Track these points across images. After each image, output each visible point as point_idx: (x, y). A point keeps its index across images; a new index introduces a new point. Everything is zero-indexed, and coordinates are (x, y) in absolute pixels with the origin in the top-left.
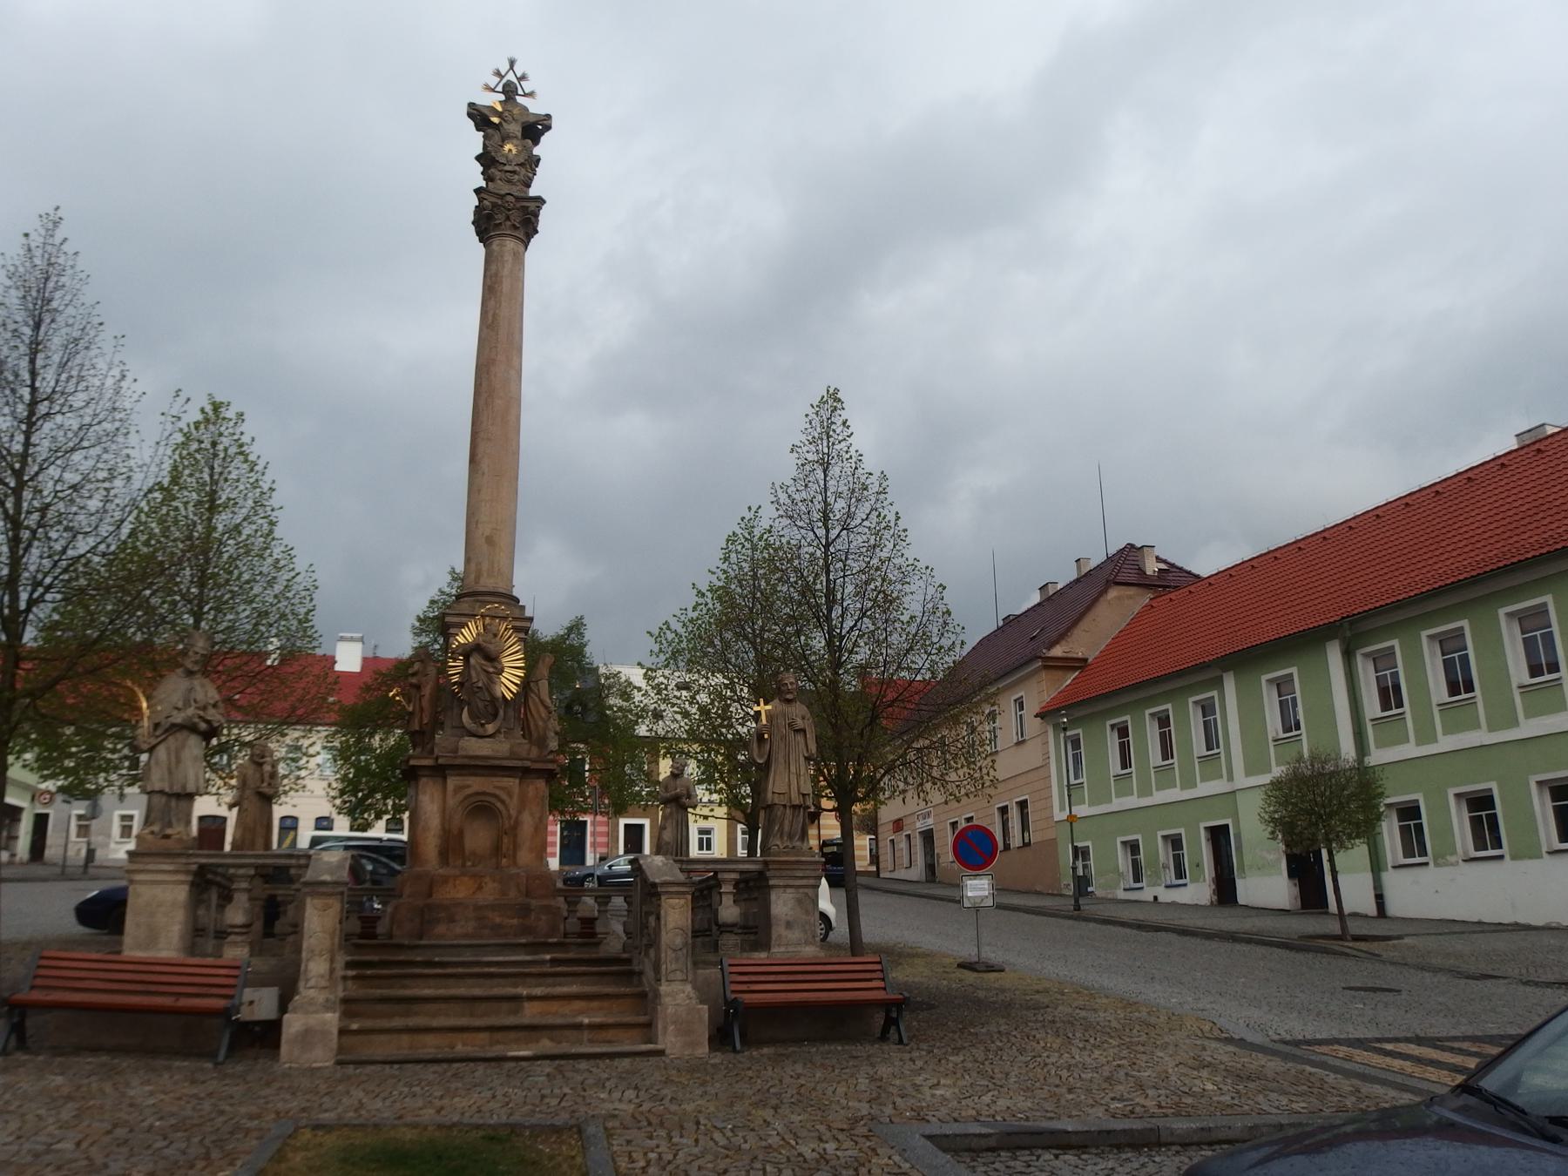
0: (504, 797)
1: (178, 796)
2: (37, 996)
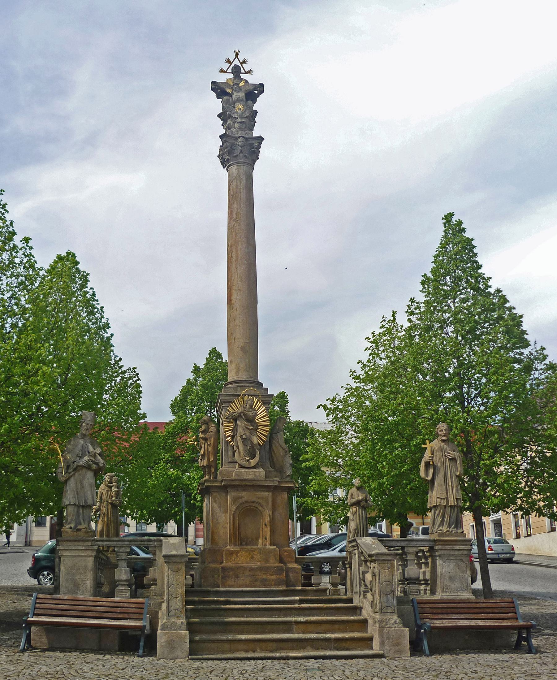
0: (263, 503)
1: (83, 507)
2: (35, 619)
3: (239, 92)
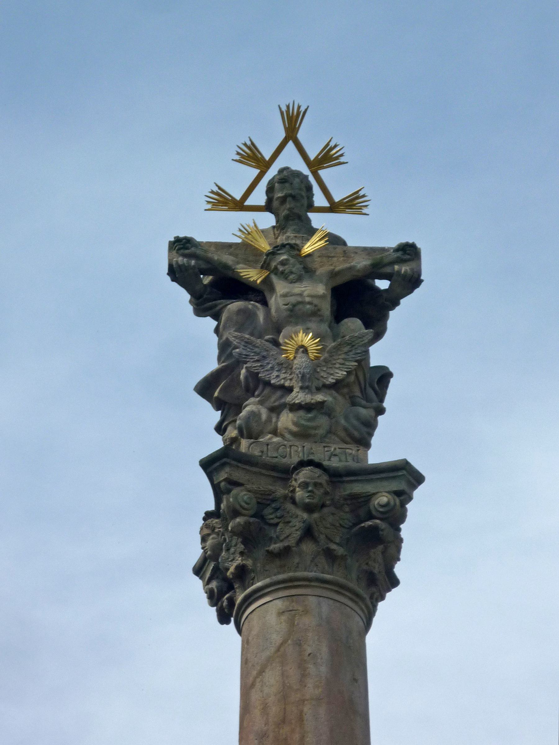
3: (299, 279)
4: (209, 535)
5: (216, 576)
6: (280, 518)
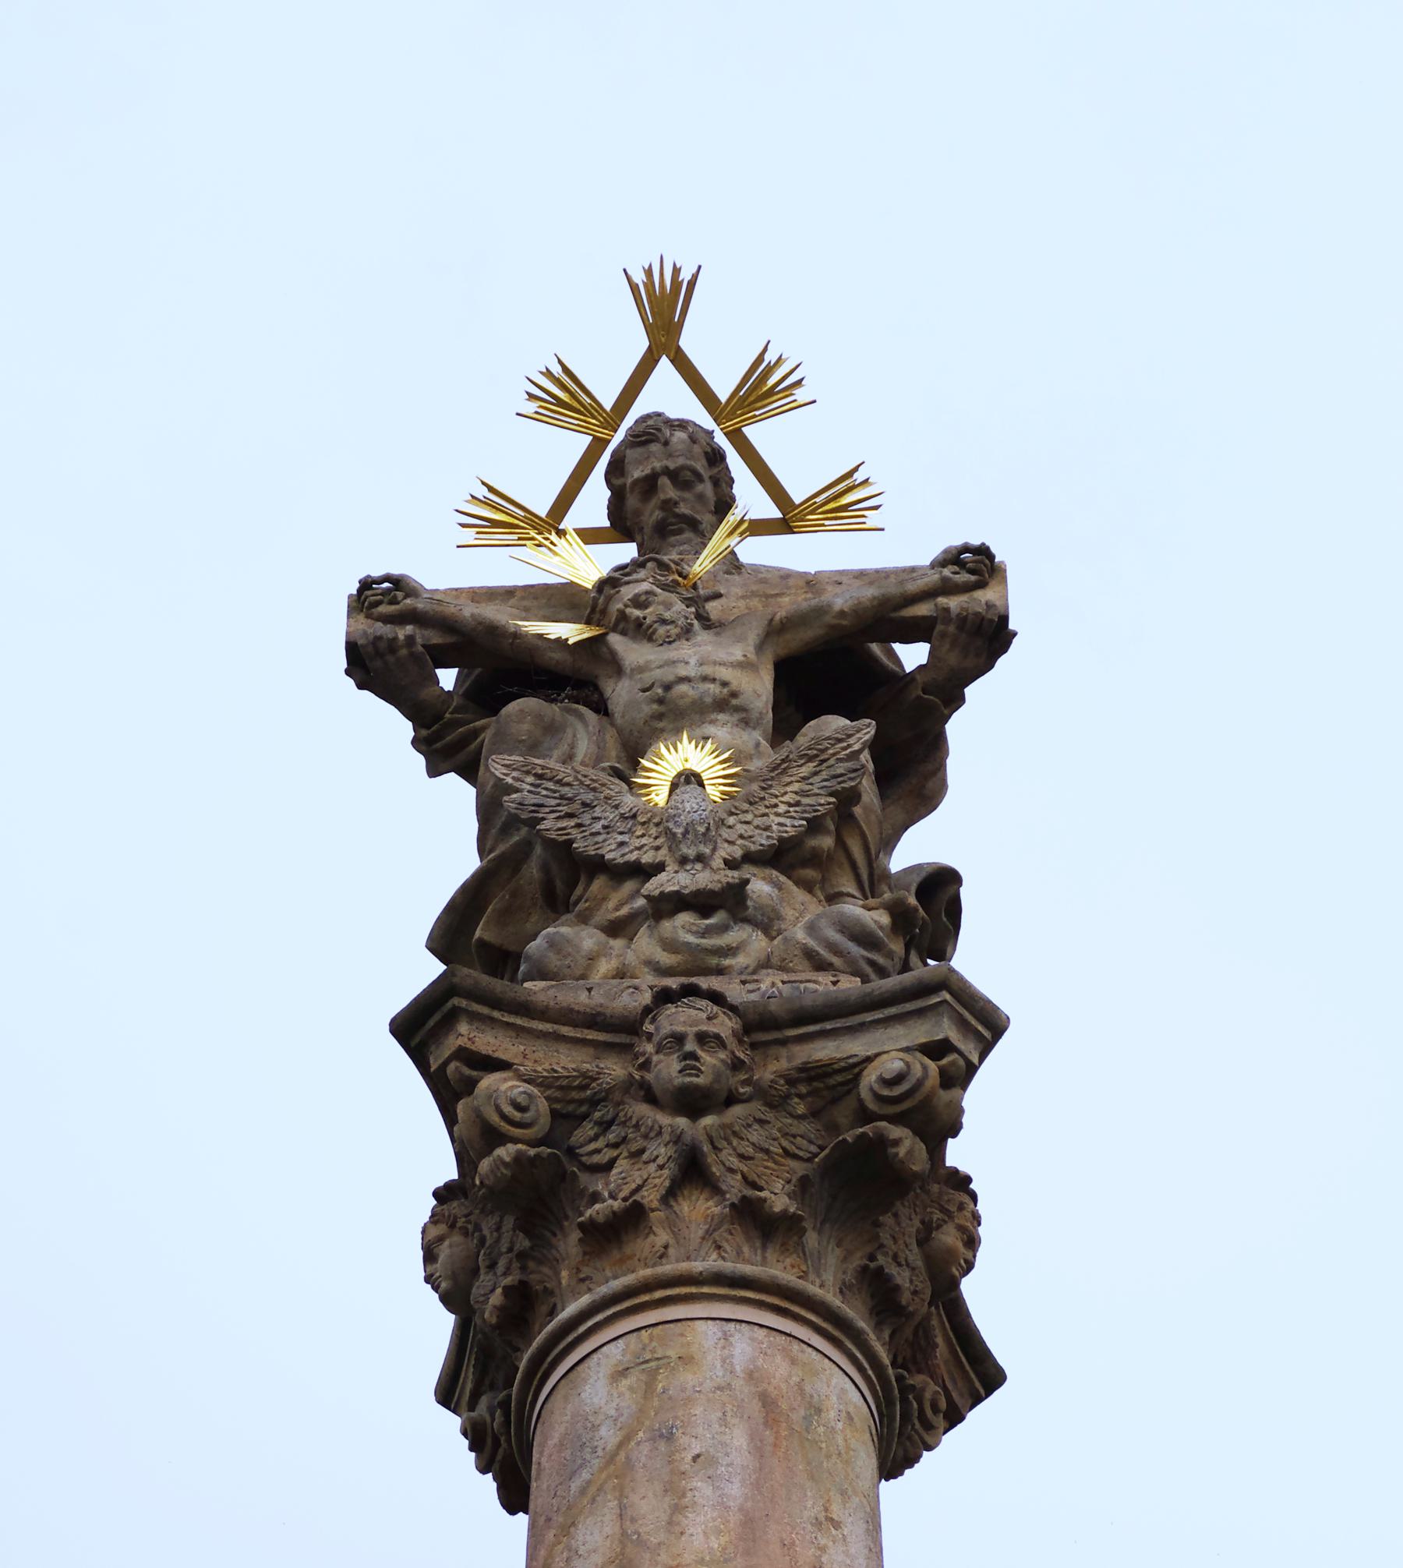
4: (440, 1239)
5: (487, 1382)
6: (616, 1146)
